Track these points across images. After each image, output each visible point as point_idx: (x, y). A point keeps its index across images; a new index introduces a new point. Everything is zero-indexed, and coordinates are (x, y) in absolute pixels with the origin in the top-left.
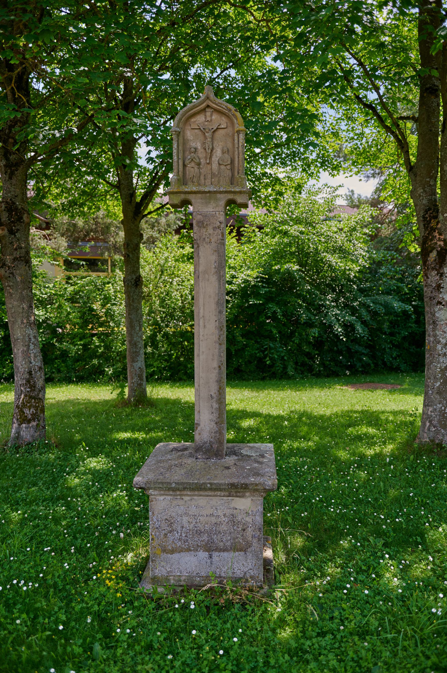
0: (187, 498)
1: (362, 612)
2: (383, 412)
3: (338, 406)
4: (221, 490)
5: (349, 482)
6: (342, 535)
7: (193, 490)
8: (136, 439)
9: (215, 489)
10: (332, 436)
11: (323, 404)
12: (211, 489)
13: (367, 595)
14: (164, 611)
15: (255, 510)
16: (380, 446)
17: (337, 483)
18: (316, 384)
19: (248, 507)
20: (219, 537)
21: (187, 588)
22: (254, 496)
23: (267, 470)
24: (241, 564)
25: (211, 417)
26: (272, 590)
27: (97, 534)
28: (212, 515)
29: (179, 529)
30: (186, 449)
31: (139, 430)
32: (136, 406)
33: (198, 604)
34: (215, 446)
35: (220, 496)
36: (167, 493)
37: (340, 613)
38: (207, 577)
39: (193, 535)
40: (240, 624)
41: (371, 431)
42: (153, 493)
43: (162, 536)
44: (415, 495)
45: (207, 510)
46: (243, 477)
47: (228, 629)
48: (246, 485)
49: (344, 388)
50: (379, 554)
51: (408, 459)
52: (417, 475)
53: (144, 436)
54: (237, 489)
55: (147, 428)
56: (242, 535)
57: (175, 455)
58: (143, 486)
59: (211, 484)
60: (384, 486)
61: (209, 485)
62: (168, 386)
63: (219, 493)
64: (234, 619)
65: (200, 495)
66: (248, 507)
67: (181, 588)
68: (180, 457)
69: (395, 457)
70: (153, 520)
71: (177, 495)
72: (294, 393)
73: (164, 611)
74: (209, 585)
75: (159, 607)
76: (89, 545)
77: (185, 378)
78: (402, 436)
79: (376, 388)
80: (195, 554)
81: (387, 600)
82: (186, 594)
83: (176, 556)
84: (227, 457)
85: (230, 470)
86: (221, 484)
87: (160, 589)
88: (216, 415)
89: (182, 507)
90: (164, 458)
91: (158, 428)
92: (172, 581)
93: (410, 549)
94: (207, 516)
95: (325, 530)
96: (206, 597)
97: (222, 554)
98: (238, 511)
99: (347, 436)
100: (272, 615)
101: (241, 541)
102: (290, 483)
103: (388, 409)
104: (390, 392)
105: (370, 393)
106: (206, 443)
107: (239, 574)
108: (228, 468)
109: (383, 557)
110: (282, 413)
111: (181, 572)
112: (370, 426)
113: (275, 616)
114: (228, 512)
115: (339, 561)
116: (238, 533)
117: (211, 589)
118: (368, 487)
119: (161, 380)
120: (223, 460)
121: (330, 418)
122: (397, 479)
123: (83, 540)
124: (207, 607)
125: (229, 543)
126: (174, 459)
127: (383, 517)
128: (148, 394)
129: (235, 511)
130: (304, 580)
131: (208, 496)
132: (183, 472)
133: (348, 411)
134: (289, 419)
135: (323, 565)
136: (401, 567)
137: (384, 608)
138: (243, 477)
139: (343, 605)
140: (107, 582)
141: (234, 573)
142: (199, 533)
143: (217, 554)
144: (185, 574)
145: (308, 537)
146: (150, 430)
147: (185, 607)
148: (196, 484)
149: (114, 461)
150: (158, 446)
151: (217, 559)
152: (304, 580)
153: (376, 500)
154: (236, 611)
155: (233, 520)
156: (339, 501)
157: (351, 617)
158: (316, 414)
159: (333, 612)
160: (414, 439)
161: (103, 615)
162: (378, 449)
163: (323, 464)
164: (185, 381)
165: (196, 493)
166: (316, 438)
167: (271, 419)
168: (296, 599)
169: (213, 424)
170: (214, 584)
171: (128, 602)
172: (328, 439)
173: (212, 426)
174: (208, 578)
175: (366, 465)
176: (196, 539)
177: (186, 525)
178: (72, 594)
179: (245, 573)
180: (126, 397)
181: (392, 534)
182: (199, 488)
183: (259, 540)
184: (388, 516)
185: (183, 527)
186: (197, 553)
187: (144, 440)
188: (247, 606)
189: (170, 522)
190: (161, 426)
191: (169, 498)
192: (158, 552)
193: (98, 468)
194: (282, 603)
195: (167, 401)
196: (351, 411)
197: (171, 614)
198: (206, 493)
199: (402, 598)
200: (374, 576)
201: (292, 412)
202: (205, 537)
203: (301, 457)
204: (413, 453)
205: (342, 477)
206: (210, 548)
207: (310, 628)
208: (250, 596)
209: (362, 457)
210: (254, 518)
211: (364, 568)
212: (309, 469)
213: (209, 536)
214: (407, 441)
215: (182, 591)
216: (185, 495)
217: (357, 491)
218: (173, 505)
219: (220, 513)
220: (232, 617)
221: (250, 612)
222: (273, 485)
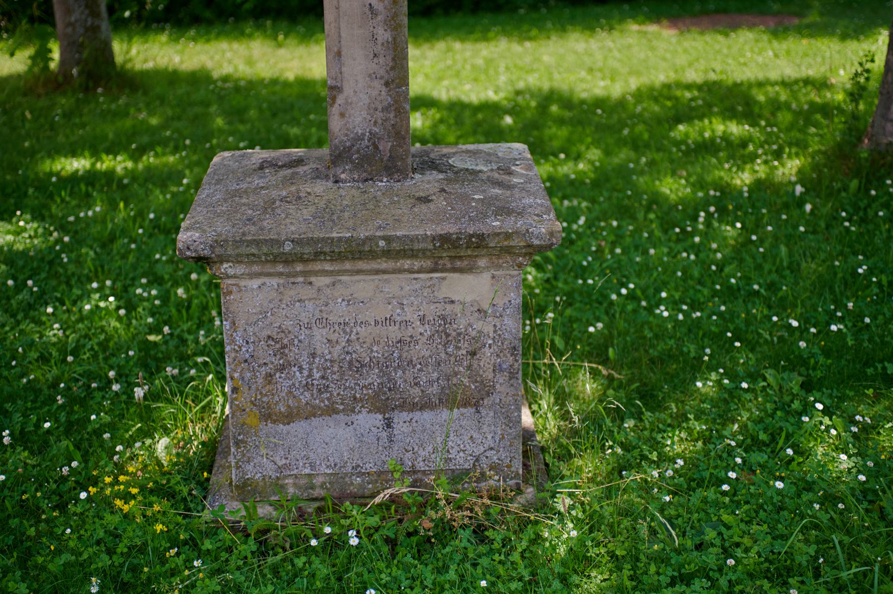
0: (321, 281)
1: (773, 528)
2: (760, 84)
3: (638, 73)
4: (413, 254)
5: (697, 249)
6: (696, 368)
7: (339, 257)
8: (109, 175)
9: (399, 251)
10: (636, 145)
11: (600, 70)
12: (387, 254)
13: (779, 492)
14: (279, 557)
15: (500, 302)
16: (766, 162)
17: (668, 254)
18: (573, 21)
19: (485, 296)
20: (409, 375)
21: (332, 504)
22: (499, 267)
23: (527, 201)
24: (466, 438)
25: (373, 67)
26: (547, 495)
27: (60, 400)
28: (390, 320)
29: (304, 360)
30: (300, 162)
31: (112, 151)
32: (86, 90)
33: (369, 533)
34: (385, 146)
35: (411, 271)
36: (269, 268)
37: (720, 534)
38: (380, 473)
39: (343, 374)
40: (479, 570)
41: (735, 129)
42: (231, 272)
43: (260, 381)
44: (870, 272)
45: (377, 306)
46: (471, 219)
47: (452, 584)
48: (481, 237)
49: (652, 28)
50: (796, 405)
51: (845, 189)
52: (871, 227)
53: (130, 164)
54: (455, 252)
55: (134, 143)
56: (469, 367)
57: (270, 177)
58: (207, 252)
59: (388, 239)
60: (791, 255)
61: (382, 243)
62: (164, 38)
63: (407, 263)
64: (462, 561)
65: (359, 272)
66: (485, 296)
67: (316, 505)
68: (290, 180)
69: (813, 182)
70: (233, 341)
71: (296, 275)
72: (516, 48)
73: (279, 557)
74: (390, 491)
75: (264, 549)
76: (47, 425)
77: (208, 14)
78: (822, 138)
79: (735, 27)
80: (348, 419)
81: (829, 500)
82: (330, 515)
83: (299, 427)
84: (417, 176)
85: (432, 206)
86: (413, 239)
87: (264, 510)
88: (385, 61)
89: (310, 305)
90: (244, 186)
91: (164, 143)
92: (291, 490)
93: (870, 392)
94: (376, 323)
95: (652, 361)
96: (383, 519)
97: (417, 415)
98: (458, 308)
99: (677, 143)
100: (554, 548)
101: (466, 381)
102: (547, 260)
103: (774, 75)
104: (775, 34)
105: (720, 38)
106: (360, 138)
107: (461, 461)
108: (426, 200)
109: (807, 409)
110: (491, 96)
111: (312, 467)
112: (731, 118)
113: (562, 550)
114: (431, 311)
115: (699, 427)
116: (458, 362)
117: (393, 499)
118: (748, 259)
119: (148, 22)
120: (408, 183)
121: (621, 103)
122: (820, 237)
123: (25, 416)
124: (392, 542)
125: (435, 389)
126: (276, 186)
127: (795, 324)
128: (119, 59)
129: (449, 307)
130: (620, 469)
131: (377, 272)
132: (306, 213)
133: (667, 86)
134: (514, 111)
135: (659, 437)
136: (855, 429)
137: (824, 518)
138: (471, 219)
139: (725, 517)
140: (118, 502)
141: (448, 460)
142: (358, 367)
143: (405, 415)
144: (324, 469)
145: (610, 378)
146: (142, 151)
147: (333, 544)
148: (348, 240)
149: (63, 228)
150: (216, 159)
151: (406, 429)
152: (620, 469)
153: (772, 287)
154: (465, 543)
155: (444, 330)
156: (677, 296)
157: (747, 541)
158: (584, 95)
159: (701, 533)
160: (860, 140)
161: (126, 577)
162: (762, 171)
163: (624, 212)
164: (210, 23)
165: (348, 265)
166: (594, 154)
167: (467, 113)
168: (608, 510)
169: (378, 84)
170: (399, 489)
171: (185, 543)
172: (623, 155)
173: (375, 93)
174: (383, 477)
175: (738, 207)
176: (350, 383)
177: (322, 348)
178: (29, 538)
179: (477, 460)
180: (53, 65)
181: (822, 359)
182: (356, 253)
183: (512, 376)
184: (806, 321)
185: (314, 355)
186: (354, 417)
187: (133, 175)
188: (489, 533)
189: (279, 344)
190: (169, 139)
191: (274, 282)
192: (252, 420)
193: (20, 247)
194: (577, 522)
195: (172, 78)
196: (679, 85)
197: (300, 562)
198: (374, 265)
199: (866, 493)
200: (790, 452)
201: (518, 93)
202: (373, 378)
203: (564, 197)
204: (857, 174)
205: (678, 241)
206: (386, 403)
207: (653, 569)
208: (495, 510)
209: (725, 190)
210: (497, 322)
211: (763, 436)
212: (589, 224)
213: (383, 373)
214: (839, 146)
215: (320, 510)
216: (316, 273)
217: (721, 269)
218: (287, 299)
219: (410, 315)
220: (458, 557)
221: (496, 546)
222: (552, 234)
